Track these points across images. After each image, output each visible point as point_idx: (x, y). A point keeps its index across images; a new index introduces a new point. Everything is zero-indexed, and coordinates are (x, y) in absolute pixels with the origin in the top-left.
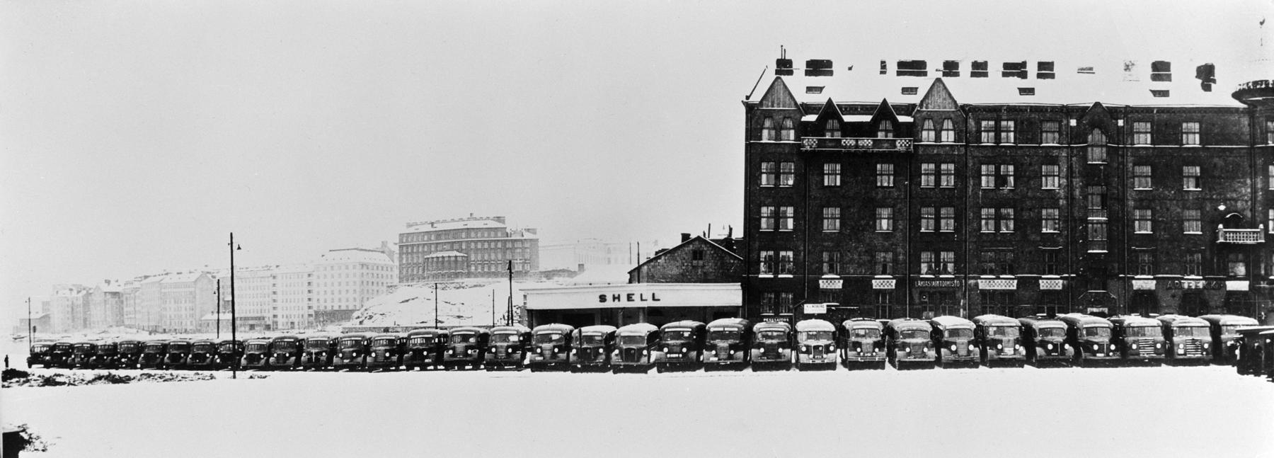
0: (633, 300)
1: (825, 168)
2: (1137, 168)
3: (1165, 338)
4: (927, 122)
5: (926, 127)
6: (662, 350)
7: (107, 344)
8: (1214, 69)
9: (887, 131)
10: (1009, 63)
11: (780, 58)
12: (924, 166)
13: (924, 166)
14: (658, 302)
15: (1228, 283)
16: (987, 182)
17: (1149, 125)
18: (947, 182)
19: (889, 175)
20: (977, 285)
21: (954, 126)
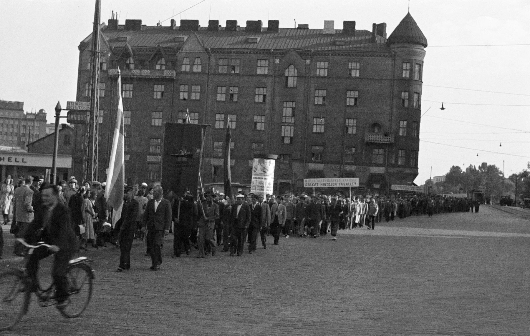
0: (11, 161)
1: (348, 94)
2: (317, 92)
3: (225, 193)
4: (185, 59)
5: (184, 63)
6: (341, 214)
7: (446, 230)
8: (386, 26)
9: (161, 65)
10: (271, 21)
11: (111, 18)
12: (182, 87)
13: (182, 87)
14: (26, 163)
15: (371, 168)
16: (221, 97)
17: (327, 63)
18: (195, 96)
19: (130, 91)
20: (209, 161)
21: (134, 61)
